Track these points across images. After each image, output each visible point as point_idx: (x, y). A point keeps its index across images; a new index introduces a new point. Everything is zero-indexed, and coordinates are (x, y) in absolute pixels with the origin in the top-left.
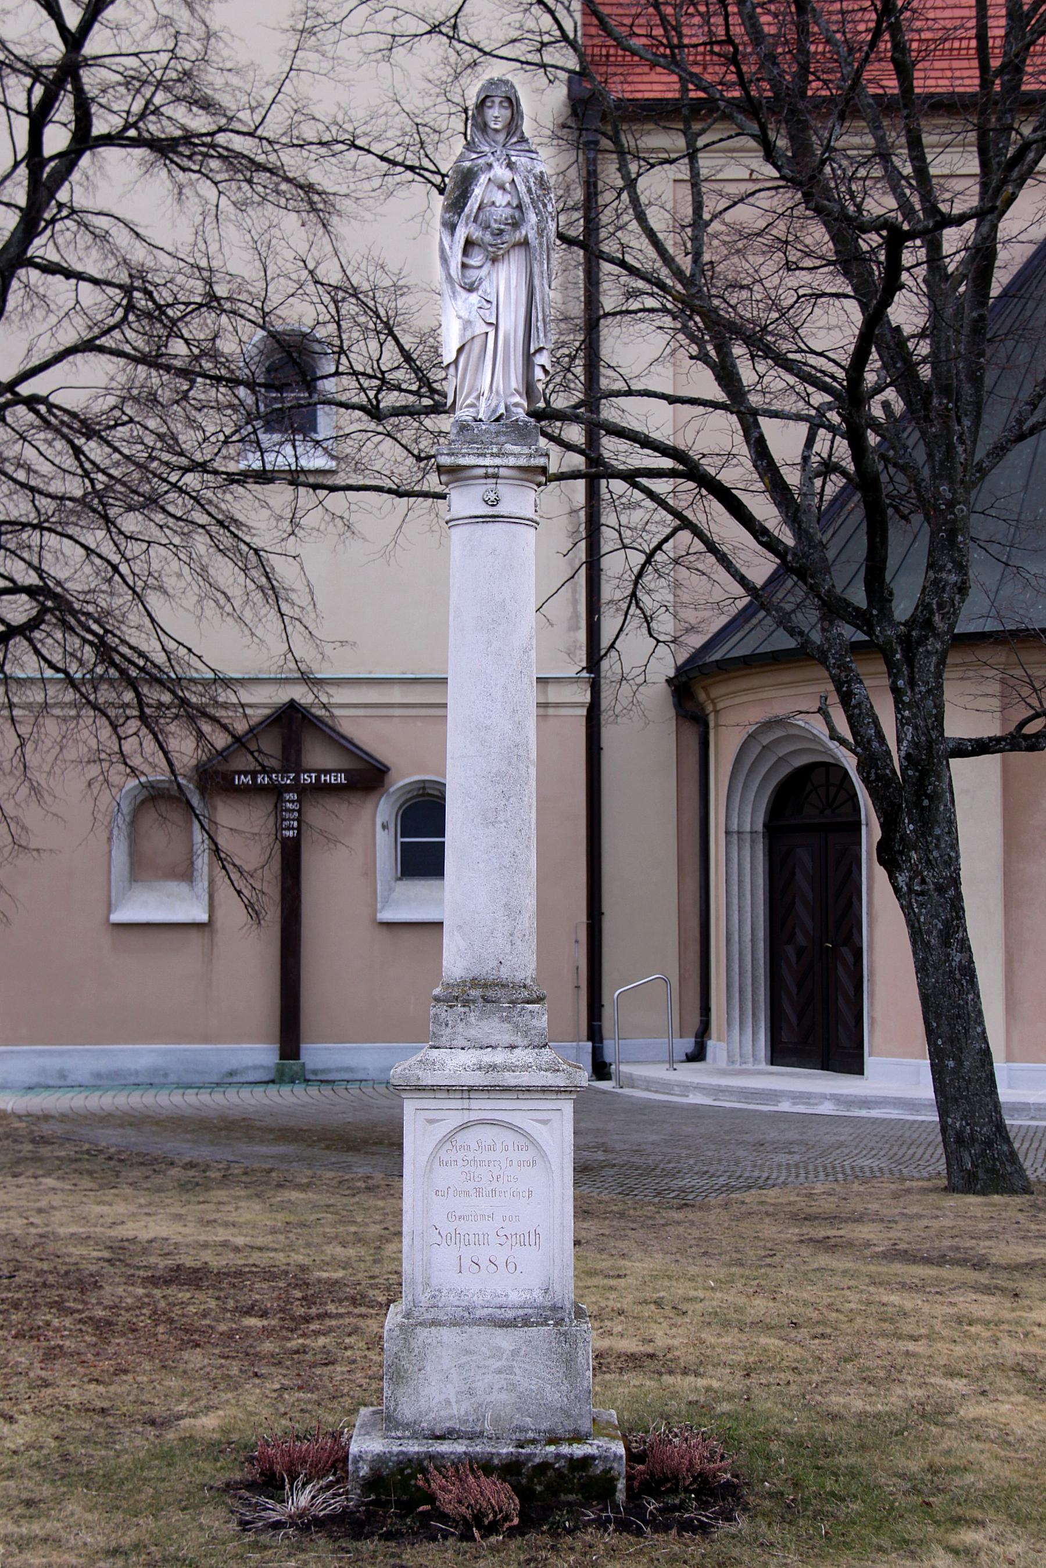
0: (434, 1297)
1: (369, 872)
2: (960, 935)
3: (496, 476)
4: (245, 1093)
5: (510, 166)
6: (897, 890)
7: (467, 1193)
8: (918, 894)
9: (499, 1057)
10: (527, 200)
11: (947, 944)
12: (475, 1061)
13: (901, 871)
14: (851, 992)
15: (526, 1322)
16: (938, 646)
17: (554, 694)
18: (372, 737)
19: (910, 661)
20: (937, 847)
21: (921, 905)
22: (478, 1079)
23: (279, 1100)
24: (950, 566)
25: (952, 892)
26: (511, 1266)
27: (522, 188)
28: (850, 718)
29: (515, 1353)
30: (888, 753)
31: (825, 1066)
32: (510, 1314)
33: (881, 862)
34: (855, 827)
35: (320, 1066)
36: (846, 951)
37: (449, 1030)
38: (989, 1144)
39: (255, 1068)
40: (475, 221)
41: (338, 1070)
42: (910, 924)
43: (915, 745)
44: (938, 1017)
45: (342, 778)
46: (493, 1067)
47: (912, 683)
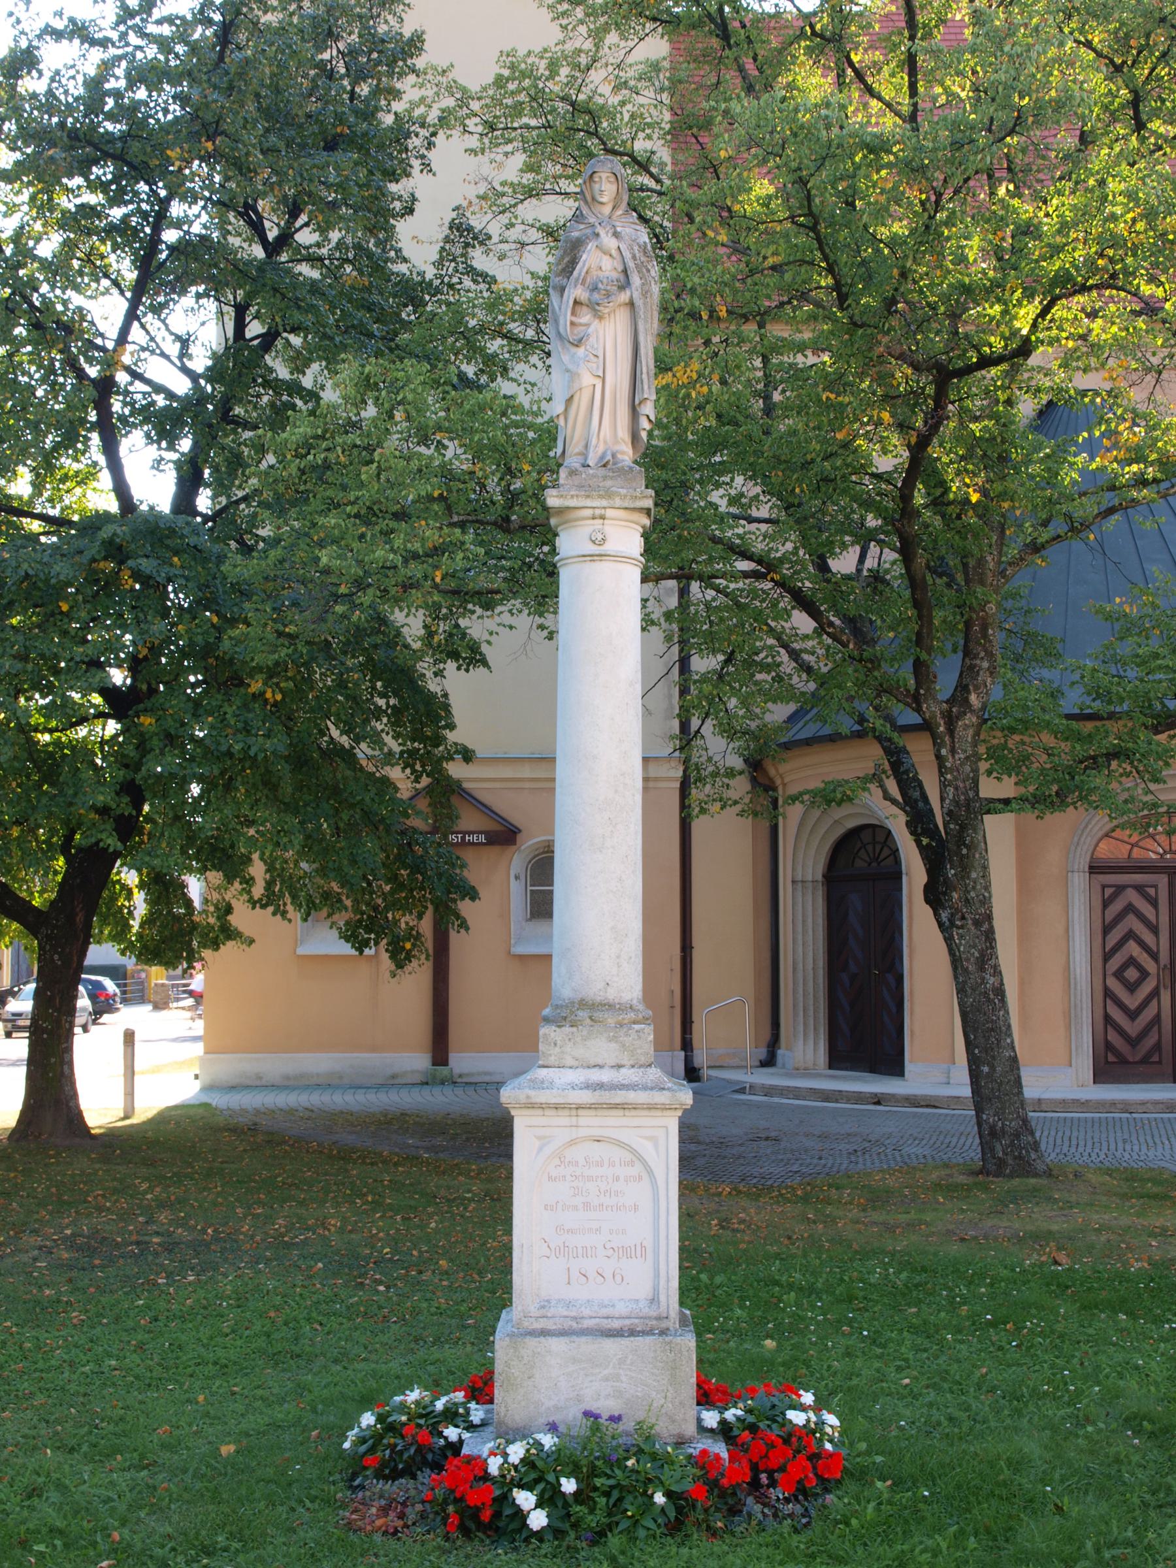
0: (543, 1307)
1: (505, 915)
2: (992, 962)
3: (603, 517)
4: (404, 1093)
5: (616, 235)
6: (940, 925)
7: (576, 1208)
8: (958, 928)
9: (605, 1076)
10: (631, 264)
11: (982, 969)
12: (582, 1079)
13: (944, 908)
14: (894, 1010)
15: (633, 1333)
16: (974, 719)
17: (654, 771)
18: (510, 807)
19: (951, 731)
20: (974, 888)
21: (961, 937)
22: (586, 1097)
23: (430, 1098)
24: (982, 654)
25: (986, 926)
26: (618, 1278)
27: (627, 255)
28: (899, 783)
29: (622, 1362)
30: (931, 810)
31: (873, 1070)
32: (616, 1324)
33: (927, 901)
34: (895, 876)
35: (466, 1071)
36: (890, 978)
37: (557, 1049)
38: (1017, 1135)
39: (413, 1072)
40: (583, 283)
41: (479, 1074)
42: (951, 952)
43: (956, 802)
44: (975, 1030)
45: (482, 838)
46: (600, 1086)
47: (953, 751)
